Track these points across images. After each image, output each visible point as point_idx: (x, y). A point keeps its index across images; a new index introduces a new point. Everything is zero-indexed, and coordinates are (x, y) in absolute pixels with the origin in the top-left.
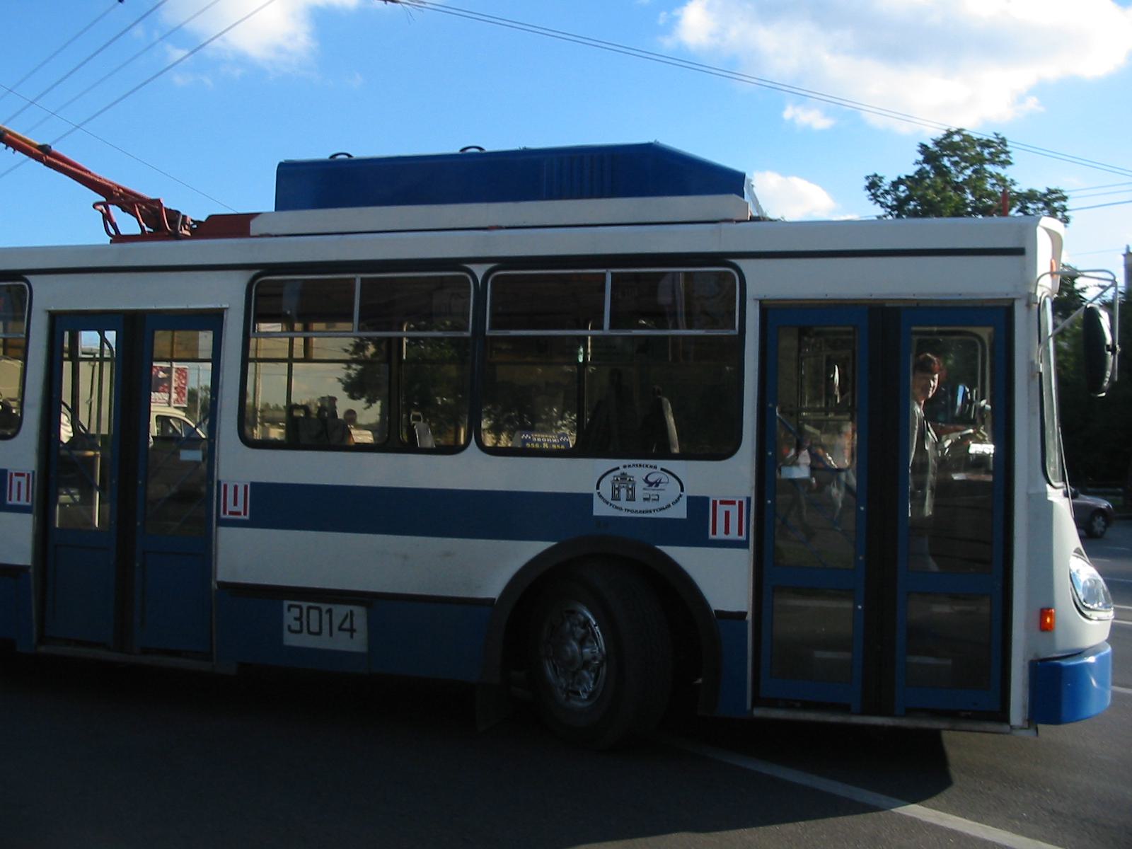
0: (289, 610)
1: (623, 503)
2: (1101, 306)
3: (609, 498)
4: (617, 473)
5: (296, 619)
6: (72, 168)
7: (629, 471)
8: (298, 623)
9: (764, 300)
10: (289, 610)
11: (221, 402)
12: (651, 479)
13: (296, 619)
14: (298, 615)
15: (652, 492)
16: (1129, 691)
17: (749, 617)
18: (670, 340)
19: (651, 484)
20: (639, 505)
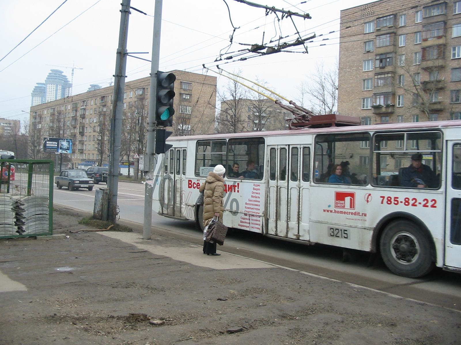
18: (415, 121)
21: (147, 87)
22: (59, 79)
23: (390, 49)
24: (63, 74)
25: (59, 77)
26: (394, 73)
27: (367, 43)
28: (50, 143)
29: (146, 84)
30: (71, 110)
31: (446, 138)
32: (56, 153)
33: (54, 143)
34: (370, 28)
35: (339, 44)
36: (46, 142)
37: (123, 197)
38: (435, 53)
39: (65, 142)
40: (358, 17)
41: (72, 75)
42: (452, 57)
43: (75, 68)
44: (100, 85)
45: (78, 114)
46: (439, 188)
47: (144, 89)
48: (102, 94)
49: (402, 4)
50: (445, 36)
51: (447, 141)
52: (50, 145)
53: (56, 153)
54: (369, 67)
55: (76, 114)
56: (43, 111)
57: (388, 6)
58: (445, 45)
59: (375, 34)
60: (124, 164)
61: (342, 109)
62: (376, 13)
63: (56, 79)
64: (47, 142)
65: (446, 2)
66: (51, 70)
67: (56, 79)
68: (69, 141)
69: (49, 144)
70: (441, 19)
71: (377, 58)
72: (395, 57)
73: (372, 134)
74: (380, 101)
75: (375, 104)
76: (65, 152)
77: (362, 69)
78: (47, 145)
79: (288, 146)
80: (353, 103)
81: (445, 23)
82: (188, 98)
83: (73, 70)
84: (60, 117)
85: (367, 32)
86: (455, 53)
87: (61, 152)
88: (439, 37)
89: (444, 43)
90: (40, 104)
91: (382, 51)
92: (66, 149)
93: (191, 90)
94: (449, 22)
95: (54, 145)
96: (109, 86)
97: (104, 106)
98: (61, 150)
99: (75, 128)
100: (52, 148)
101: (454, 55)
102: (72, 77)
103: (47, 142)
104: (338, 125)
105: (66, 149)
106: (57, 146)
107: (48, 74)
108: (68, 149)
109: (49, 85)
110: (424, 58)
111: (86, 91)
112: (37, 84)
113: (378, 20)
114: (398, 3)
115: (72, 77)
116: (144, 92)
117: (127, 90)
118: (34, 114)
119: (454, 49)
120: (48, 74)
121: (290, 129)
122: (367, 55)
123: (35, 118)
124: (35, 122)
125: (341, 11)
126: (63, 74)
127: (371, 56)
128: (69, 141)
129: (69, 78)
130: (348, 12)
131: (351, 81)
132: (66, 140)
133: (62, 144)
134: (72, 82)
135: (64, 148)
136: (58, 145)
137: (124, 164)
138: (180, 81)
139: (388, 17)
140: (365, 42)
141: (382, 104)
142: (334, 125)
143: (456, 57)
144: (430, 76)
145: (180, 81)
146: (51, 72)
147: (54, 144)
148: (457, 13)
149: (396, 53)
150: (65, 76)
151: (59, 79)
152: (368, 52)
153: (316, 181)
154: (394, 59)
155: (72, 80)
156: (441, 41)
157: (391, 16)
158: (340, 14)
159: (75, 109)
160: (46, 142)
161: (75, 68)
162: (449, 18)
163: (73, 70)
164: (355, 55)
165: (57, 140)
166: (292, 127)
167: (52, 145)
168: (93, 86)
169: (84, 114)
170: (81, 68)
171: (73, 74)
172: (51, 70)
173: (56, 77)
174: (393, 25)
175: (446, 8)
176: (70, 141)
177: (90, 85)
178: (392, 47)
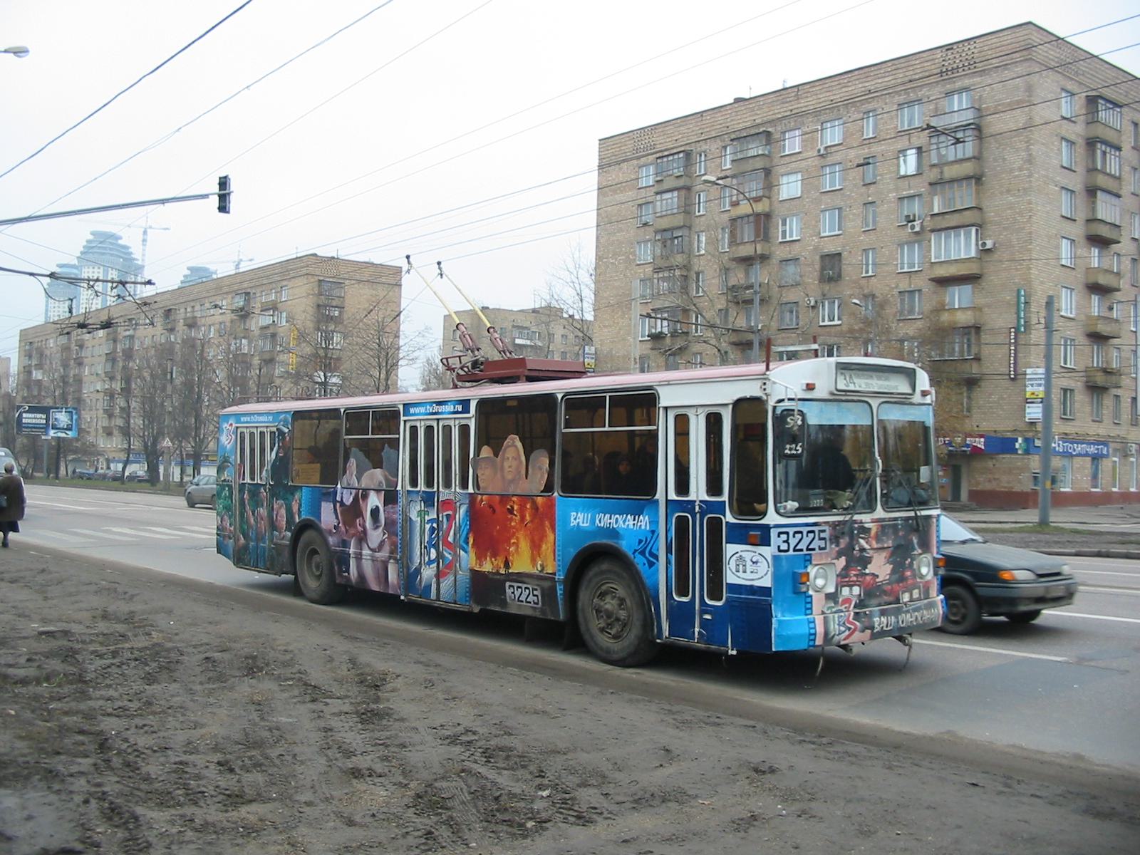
0: (794, 537)
1: (740, 574)
2: (898, 457)
3: (734, 571)
4: (737, 555)
5: (784, 542)
6: (158, 536)
7: (744, 554)
8: (786, 544)
9: (840, 261)
10: (794, 537)
11: (408, 640)
12: (754, 560)
13: (784, 542)
14: (785, 539)
15: (754, 567)
16: (1138, 621)
17: (1049, 505)
18: (826, 354)
19: (754, 563)
20: (748, 575)
21: (254, 291)
22: (112, 255)
23: (679, 220)
24: (120, 242)
25: (111, 249)
26: (687, 267)
27: (644, 206)
28: (30, 415)
29: (251, 285)
30: (104, 339)
31: (663, 402)
32: (43, 437)
33: (39, 416)
34: (648, 177)
35: (596, 212)
36: (20, 415)
37: (32, 506)
38: (747, 233)
39: (64, 413)
40: (836, 83)
41: (143, 245)
42: (780, 237)
43: (150, 227)
44: (212, 268)
45: (119, 348)
46: (708, 495)
47: (248, 294)
48: (168, 303)
49: (700, 131)
50: (769, 198)
51: (666, 408)
52: (29, 421)
53: (43, 437)
54: (646, 254)
55: (115, 349)
56: (47, 340)
57: (677, 133)
58: (768, 216)
59: (654, 189)
60: (210, 459)
61: (601, 340)
62: (658, 148)
63: (103, 254)
64: (24, 415)
65: (769, 132)
66: (92, 233)
67: (103, 254)
68: (72, 412)
69: (28, 418)
70: (759, 164)
71: (657, 238)
72: (689, 237)
73: (560, 396)
74: (662, 327)
75: (653, 331)
76: (64, 435)
77: (635, 260)
78: (24, 421)
79: (436, 422)
80: (620, 329)
81: (768, 172)
82: (337, 313)
83: (145, 233)
84: (83, 355)
85: (644, 185)
86: (786, 231)
87: (55, 435)
88: (758, 199)
89: (767, 210)
90: (99, 307)
91: (664, 223)
92: (66, 429)
93: (343, 298)
94: (774, 170)
95: (38, 421)
96: (233, 272)
97: (172, 330)
98: (54, 431)
99: (112, 379)
100: (35, 426)
101: (784, 233)
102: (144, 250)
103: (24, 415)
104: (531, 379)
105: (66, 429)
106: (44, 422)
107: (85, 243)
108: (70, 429)
109: (86, 270)
110: (733, 242)
111: (176, 287)
112: (58, 266)
113: (659, 161)
114: (694, 129)
115: (144, 250)
116: (247, 301)
117: (216, 297)
118: (27, 347)
119: (784, 223)
120: (85, 243)
121: (456, 387)
122: (643, 229)
123: (30, 357)
124: (30, 366)
125: (600, 140)
126: (120, 242)
127: (649, 234)
128: (72, 412)
129: (136, 252)
130: (610, 142)
131: (617, 284)
132: (64, 410)
133: (56, 419)
134: (143, 260)
135: (61, 426)
136: (47, 419)
137: (210, 459)
138: (317, 278)
139: (676, 157)
140: (640, 205)
141: (665, 330)
142: (524, 378)
143: (788, 239)
144: (747, 274)
145: (317, 278)
146: (91, 237)
147: (39, 419)
148: (787, 153)
149: (690, 228)
150: (126, 247)
151: (112, 255)
152: (645, 224)
153: (563, 492)
154: (686, 239)
155: (144, 255)
156: (760, 208)
157: (681, 155)
158: (598, 146)
159: (111, 336)
160: (20, 415)
161: (150, 227)
162: (776, 161)
163: (145, 233)
164: (623, 231)
165: (45, 410)
166: (460, 384)
167: (34, 421)
168: (193, 270)
169: (131, 349)
170: (166, 227)
171: (144, 240)
172: (92, 233)
173: (105, 248)
174: (682, 173)
175: (768, 142)
176: (74, 412)
177: (188, 269)
178: (681, 217)
